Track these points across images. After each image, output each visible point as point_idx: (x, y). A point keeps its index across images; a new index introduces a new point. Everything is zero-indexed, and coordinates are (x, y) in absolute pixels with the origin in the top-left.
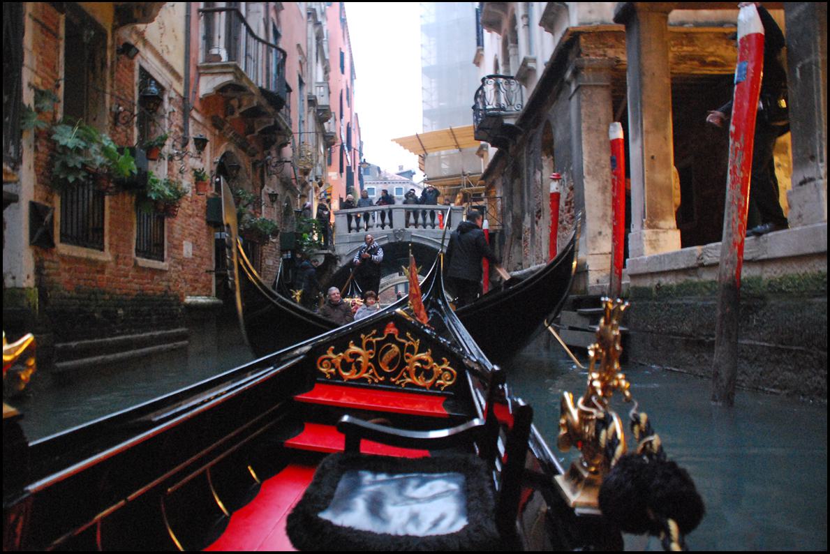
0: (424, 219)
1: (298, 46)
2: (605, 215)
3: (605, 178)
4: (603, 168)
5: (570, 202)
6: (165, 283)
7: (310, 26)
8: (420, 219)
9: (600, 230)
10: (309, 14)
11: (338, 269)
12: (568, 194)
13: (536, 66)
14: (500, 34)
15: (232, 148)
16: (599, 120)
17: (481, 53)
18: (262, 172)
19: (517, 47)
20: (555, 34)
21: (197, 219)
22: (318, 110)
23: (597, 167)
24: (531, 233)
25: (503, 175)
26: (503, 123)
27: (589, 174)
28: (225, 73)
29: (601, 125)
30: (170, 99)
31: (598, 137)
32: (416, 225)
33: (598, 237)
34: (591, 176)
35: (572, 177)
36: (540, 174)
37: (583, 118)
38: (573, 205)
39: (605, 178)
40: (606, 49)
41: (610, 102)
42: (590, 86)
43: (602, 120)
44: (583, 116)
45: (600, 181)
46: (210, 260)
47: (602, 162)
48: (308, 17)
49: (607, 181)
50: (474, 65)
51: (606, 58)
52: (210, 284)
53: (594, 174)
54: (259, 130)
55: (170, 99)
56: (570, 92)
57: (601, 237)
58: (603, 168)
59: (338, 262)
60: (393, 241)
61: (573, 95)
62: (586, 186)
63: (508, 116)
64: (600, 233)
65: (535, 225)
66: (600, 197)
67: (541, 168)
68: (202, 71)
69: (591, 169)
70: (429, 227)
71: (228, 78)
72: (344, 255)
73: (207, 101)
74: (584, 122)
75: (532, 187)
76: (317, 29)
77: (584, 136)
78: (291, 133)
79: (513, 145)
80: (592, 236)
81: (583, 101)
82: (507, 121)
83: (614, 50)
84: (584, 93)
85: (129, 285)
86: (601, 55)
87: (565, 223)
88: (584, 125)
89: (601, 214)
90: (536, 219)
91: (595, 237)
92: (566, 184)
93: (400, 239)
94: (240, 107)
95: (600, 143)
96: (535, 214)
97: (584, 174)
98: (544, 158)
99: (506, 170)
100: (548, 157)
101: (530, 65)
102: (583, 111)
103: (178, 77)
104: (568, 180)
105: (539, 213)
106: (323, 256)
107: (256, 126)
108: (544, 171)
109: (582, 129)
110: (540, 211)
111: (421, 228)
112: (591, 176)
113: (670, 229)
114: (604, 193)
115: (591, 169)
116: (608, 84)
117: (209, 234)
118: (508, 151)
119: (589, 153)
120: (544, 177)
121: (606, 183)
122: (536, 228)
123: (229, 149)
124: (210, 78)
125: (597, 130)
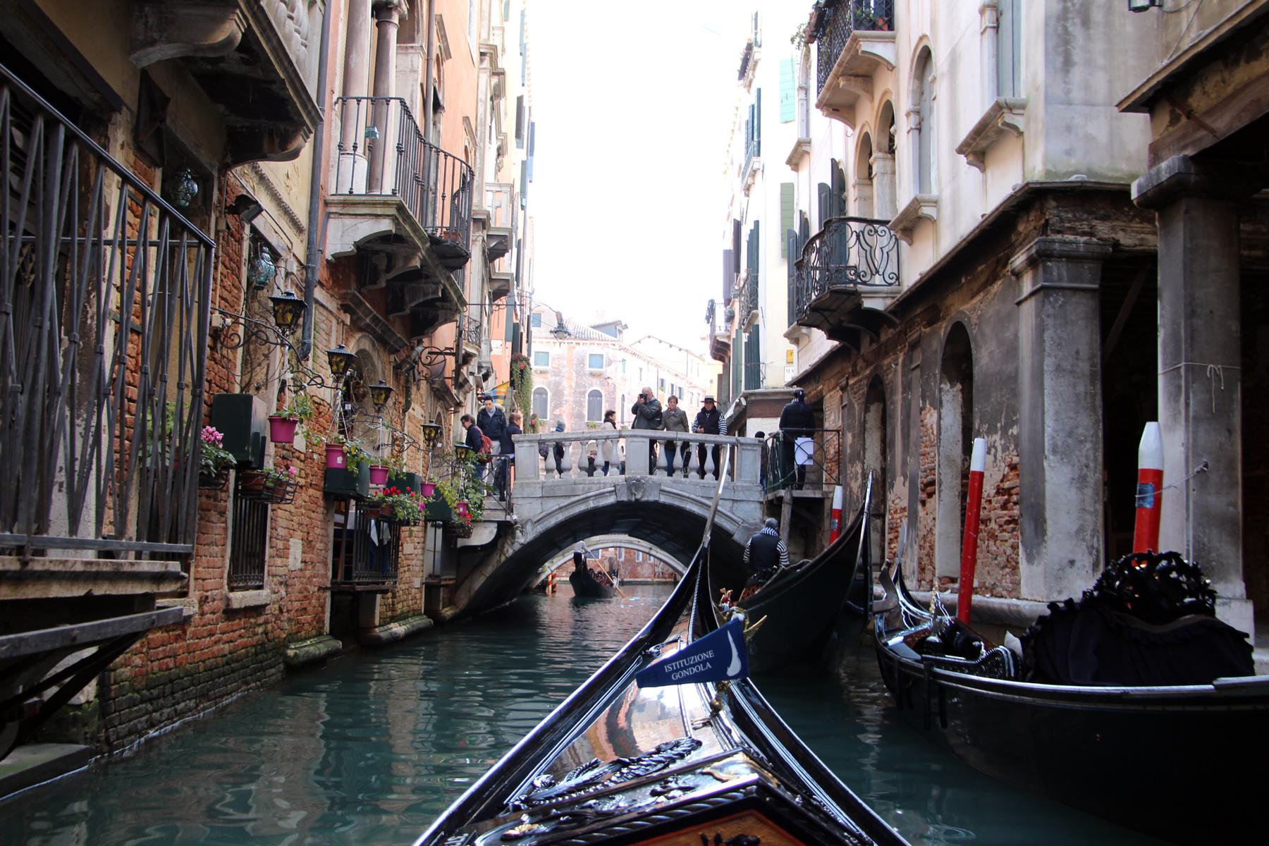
0: (687, 458)
1: (466, 119)
2: (1081, 530)
3: (1084, 460)
4: (1081, 442)
5: (1008, 492)
6: (260, 630)
7: (484, 77)
8: (678, 460)
9: (1071, 557)
10: (482, 54)
11: (517, 547)
12: (1004, 476)
13: (938, 212)
14: (853, 127)
15: (366, 345)
16: (1077, 352)
17: (804, 148)
18: (407, 381)
19: (894, 159)
20: (989, 172)
21: (311, 491)
22: (488, 236)
23: (1070, 441)
24: (909, 517)
25: (843, 389)
26: (860, 305)
27: (1054, 452)
28: (377, 216)
29: (1081, 364)
30: (288, 274)
31: (1074, 386)
32: (670, 470)
33: (1068, 570)
34: (1059, 457)
35: (1016, 446)
36: (935, 415)
37: (1047, 349)
38: (1015, 498)
39: (1084, 460)
40: (1094, 222)
41: (1097, 322)
42: (1063, 289)
43: (1081, 354)
44: (1047, 344)
45: (1073, 466)
46: (325, 564)
47: (1080, 431)
48: (482, 61)
49: (1087, 466)
50: (788, 167)
51: (1094, 240)
52: (323, 612)
53: (1063, 452)
54: (413, 304)
55: (288, 274)
56: (1020, 291)
57: (1075, 569)
58: (1081, 442)
59: (518, 533)
60: (625, 499)
61: (1026, 299)
62: (1049, 474)
63: (873, 295)
64: (1072, 563)
65: (920, 507)
66: (1072, 494)
67: (938, 405)
68: (333, 209)
69: (1060, 443)
70: (694, 476)
71: (385, 226)
72: (530, 520)
73: (339, 264)
74: (1049, 355)
75: (913, 433)
76: (495, 80)
77: (1048, 382)
78: (464, 303)
79: (872, 341)
80: (1057, 567)
81: (1048, 316)
82: (868, 304)
83: (1109, 224)
84: (1050, 302)
85: (215, 648)
86: (1084, 234)
87: (993, 525)
88: (1049, 363)
89: (1075, 527)
90: (922, 496)
91: (1062, 569)
92: (999, 454)
93: (638, 497)
94: (388, 270)
95: (1077, 395)
96: (920, 486)
97: (1046, 452)
98: (946, 386)
99: (851, 382)
100: (952, 387)
101: (927, 211)
102: (1047, 335)
103: (299, 230)
104: (1005, 448)
105: (929, 488)
106: (496, 525)
107: (407, 298)
108: (943, 411)
109: (1045, 368)
110: (932, 483)
111: (678, 475)
112: (1059, 457)
113: (1235, 599)
114: (1080, 489)
115: (1060, 443)
116: (1096, 286)
117: (326, 521)
118: (858, 349)
119: (1057, 413)
120: (944, 423)
121: (1085, 470)
122: (921, 513)
123: (362, 347)
124: (348, 221)
125: (1072, 372)
